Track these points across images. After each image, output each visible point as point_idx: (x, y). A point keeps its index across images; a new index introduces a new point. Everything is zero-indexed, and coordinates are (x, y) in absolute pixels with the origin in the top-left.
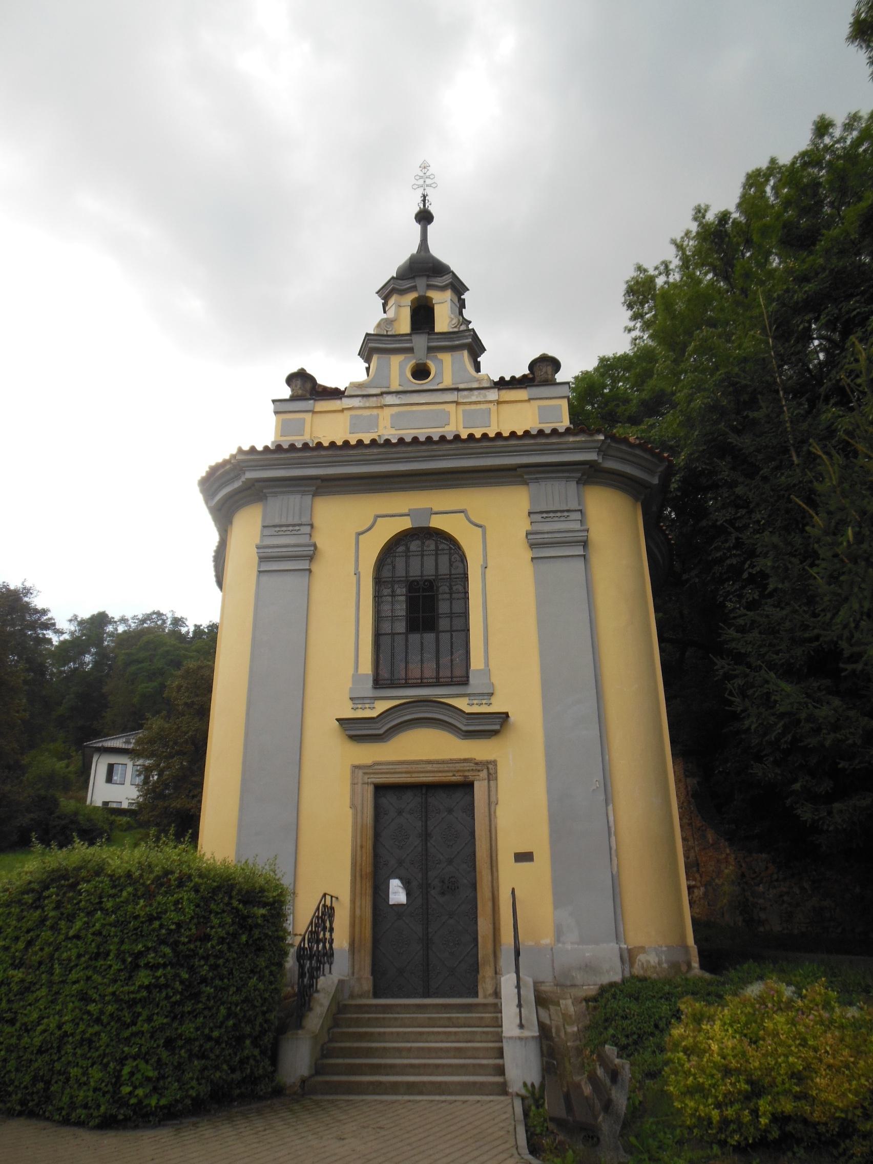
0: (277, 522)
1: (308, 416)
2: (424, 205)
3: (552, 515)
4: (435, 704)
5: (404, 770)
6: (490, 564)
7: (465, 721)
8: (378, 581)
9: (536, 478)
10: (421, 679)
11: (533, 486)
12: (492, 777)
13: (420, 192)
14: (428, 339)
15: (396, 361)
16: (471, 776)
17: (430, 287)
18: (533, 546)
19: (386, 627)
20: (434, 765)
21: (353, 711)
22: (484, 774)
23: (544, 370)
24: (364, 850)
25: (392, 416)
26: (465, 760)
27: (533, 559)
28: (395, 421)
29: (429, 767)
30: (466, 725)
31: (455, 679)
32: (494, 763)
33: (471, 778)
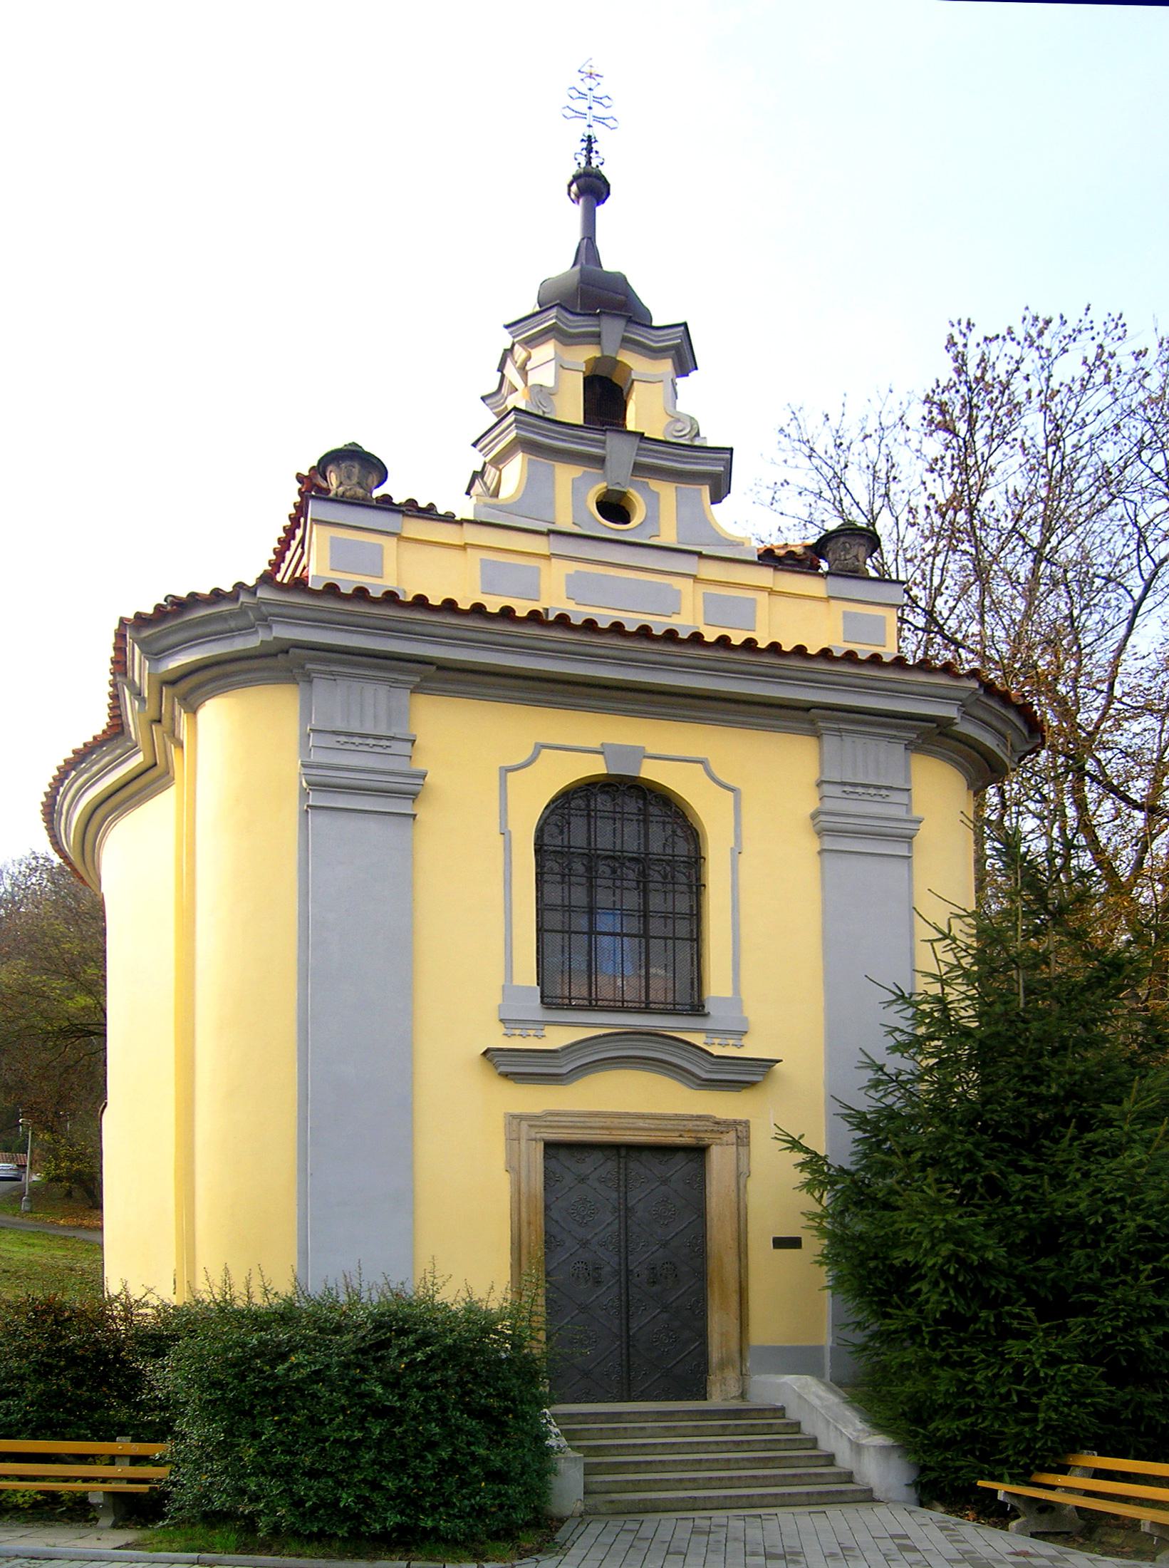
0: (340, 725)
1: (389, 544)
2: (589, 162)
3: (860, 790)
4: (660, 1039)
5: (598, 1125)
6: (747, 848)
7: (709, 1067)
8: (540, 849)
9: (839, 730)
10: (623, 1002)
11: (830, 742)
12: (743, 1140)
13: (579, 129)
14: (639, 449)
15: (566, 475)
16: (707, 1138)
17: (627, 343)
18: (821, 833)
19: (683, 928)
20: (648, 1121)
21: (505, 1037)
22: (731, 1137)
23: (853, 552)
24: (532, 1227)
25: (568, 576)
26: (699, 1118)
27: (822, 852)
28: (574, 587)
29: (641, 1123)
30: (707, 1072)
31: (677, 1007)
32: (746, 1124)
33: (707, 1142)
